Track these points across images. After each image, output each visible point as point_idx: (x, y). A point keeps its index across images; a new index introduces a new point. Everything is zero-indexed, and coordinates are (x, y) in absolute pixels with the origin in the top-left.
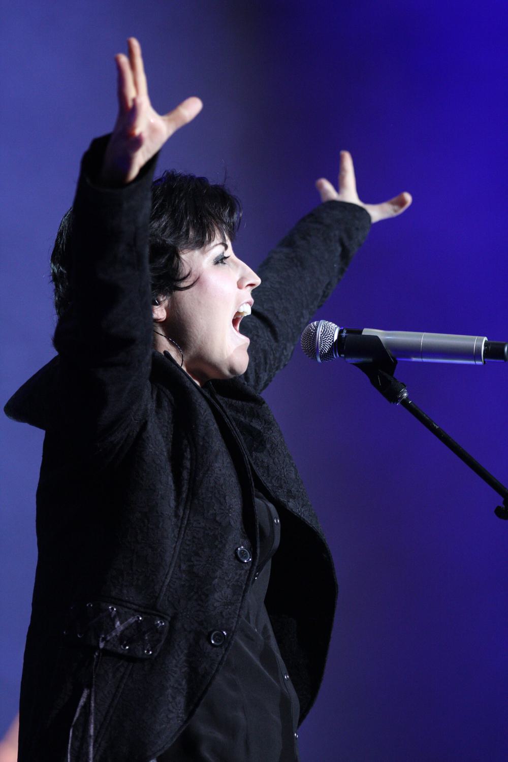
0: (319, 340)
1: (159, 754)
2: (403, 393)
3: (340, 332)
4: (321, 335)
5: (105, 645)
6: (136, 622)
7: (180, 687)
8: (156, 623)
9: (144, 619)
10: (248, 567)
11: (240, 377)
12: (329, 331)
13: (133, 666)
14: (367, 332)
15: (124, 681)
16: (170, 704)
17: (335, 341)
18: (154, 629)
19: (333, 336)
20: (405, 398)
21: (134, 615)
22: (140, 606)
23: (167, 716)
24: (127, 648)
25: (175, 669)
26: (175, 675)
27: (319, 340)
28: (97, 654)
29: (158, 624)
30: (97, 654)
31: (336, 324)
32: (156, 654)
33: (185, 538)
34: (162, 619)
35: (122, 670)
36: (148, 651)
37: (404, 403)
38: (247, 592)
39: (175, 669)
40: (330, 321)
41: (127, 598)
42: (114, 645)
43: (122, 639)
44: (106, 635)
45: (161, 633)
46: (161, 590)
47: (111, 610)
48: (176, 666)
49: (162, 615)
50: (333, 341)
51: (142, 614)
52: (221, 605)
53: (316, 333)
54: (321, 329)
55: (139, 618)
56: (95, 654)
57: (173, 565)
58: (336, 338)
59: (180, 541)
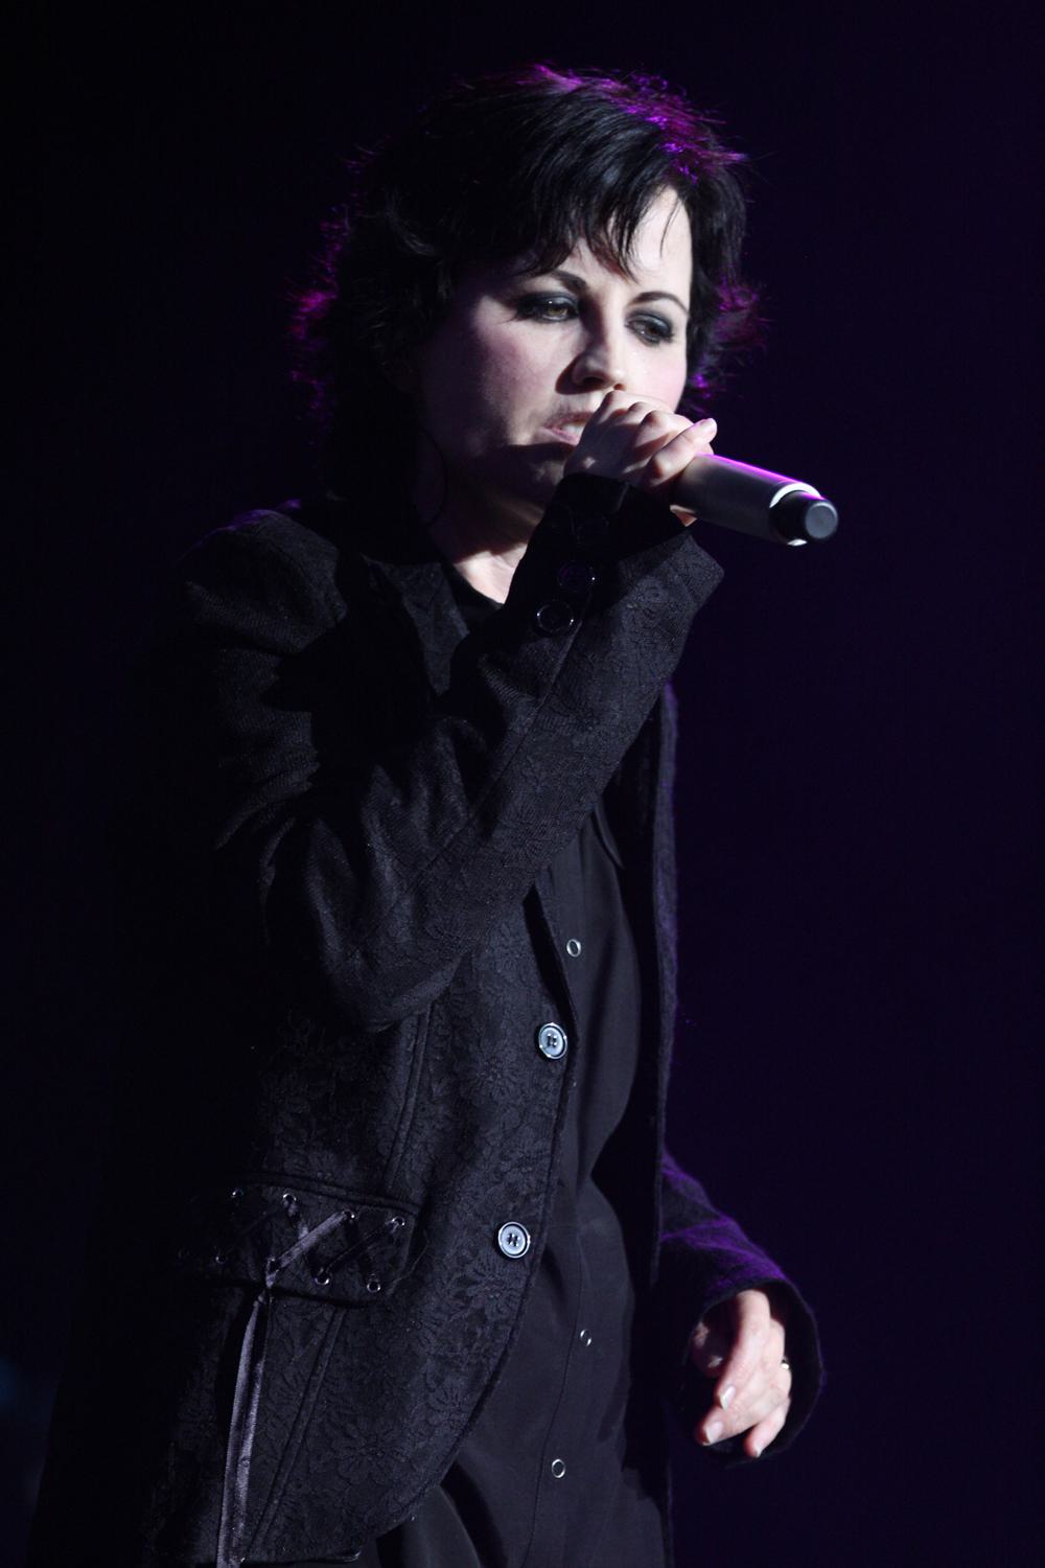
1: (559, 431)
5: (277, 1280)
6: (344, 1223)
7: (450, 1355)
8: (387, 1223)
9: (362, 1217)
10: (558, 1070)
11: (586, 362)
13: (345, 1315)
15: (328, 1351)
16: (431, 1395)
18: (382, 1234)
21: (339, 1211)
22: (349, 1189)
23: (426, 1421)
24: (327, 1282)
25: (438, 1316)
26: (439, 1330)
28: (261, 1299)
29: (392, 1225)
30: (261, 1299)
32: (390, 1291)
33: (435, 1024)
34: (401, 1213)
35: (322, 1327)
36: (374, 1286)
38: (562, 1128)
39: (438, 1316)
41: (319, 1174)
42: (298, 1278)
43: (312, 1258)
44: (277, 1256)
45: (399, 1244)
46: (393, 1151)
47: (286, 1203)
48: (439, 1309)
49: (400, 1204)
52: (512, 1167)
55: (349, 1215)
56: (257, 1299)
57: (415, 1090)
59: (425, 1029)
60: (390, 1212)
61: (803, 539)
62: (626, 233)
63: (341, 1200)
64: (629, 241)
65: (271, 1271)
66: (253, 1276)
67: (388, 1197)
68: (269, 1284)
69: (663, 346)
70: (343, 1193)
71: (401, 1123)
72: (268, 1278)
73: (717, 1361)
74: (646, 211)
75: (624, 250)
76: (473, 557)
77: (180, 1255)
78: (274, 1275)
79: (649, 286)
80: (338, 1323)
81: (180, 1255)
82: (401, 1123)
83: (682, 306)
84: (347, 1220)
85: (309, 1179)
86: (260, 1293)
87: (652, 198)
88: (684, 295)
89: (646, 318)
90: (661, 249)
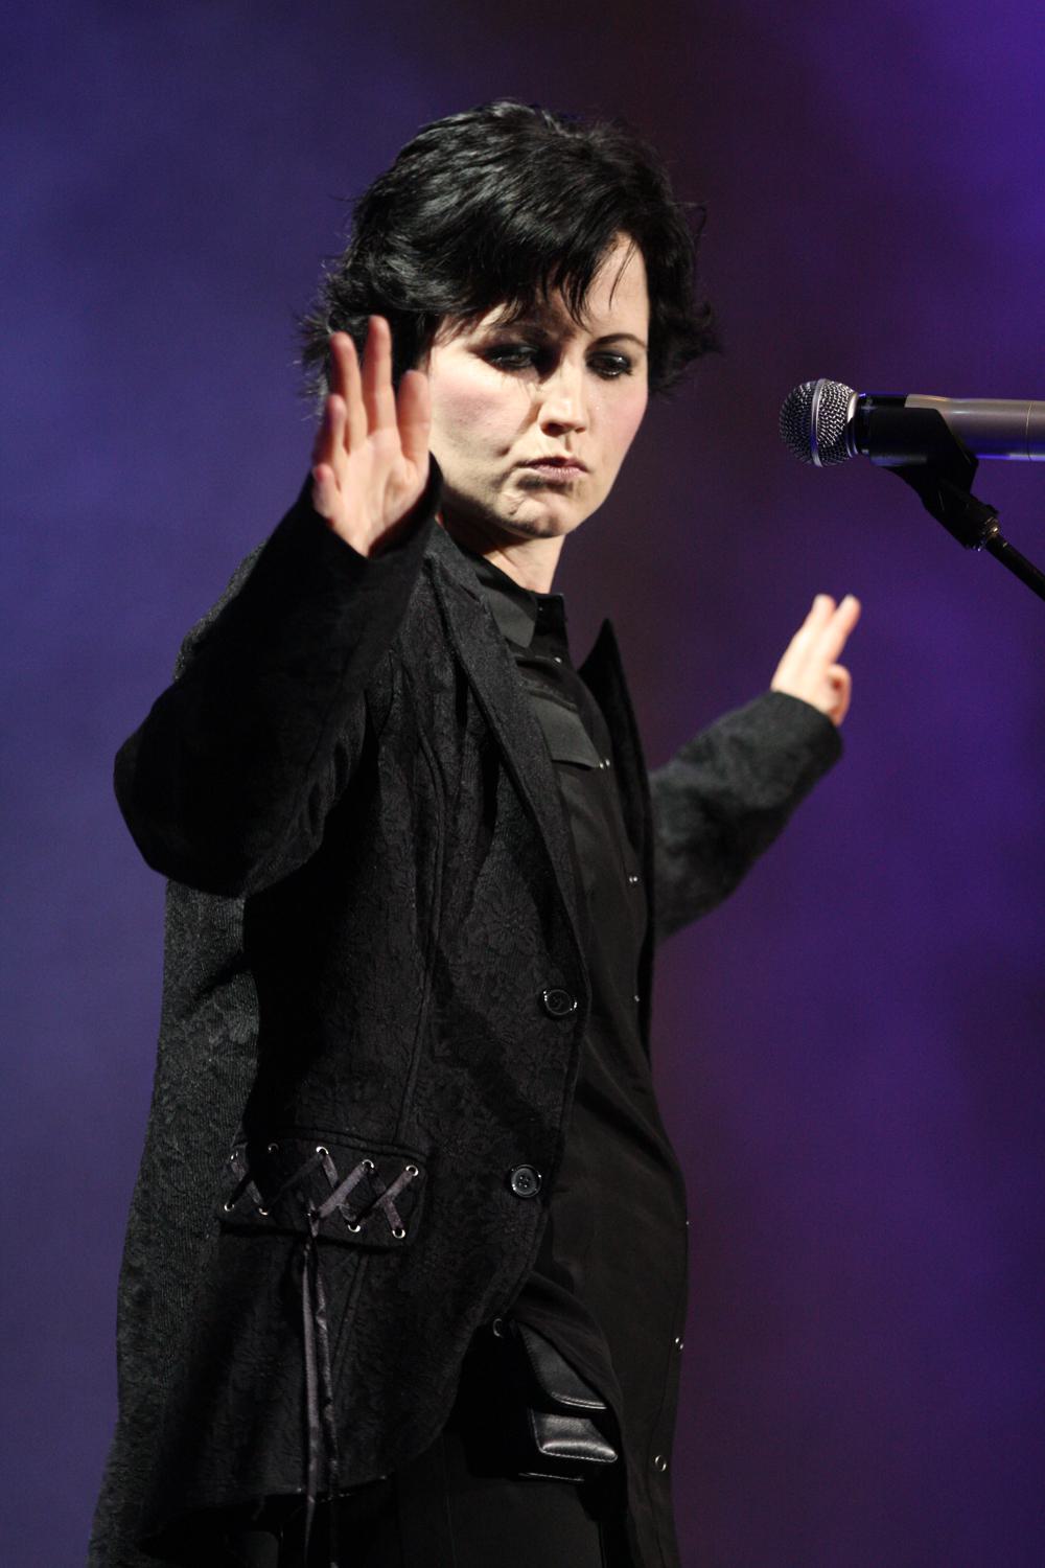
0: (817, 419)
2: (992, 525)
3: (860, 402)
4: (821, 409)
5: (320, 1229)
12: (835, 401)
14: (915, 401)
17: (849, 420)
19: (846, 412)
20: (994, 535)
27: (817, 419)
28: (308, 1247)
30: (308, 1247)
31: (851, 387)
37: (994, 546)
40: (847, 384)
50: (845, 421)
51: (373, 1156)
53: (810, 405)
54: (820, 397)
58: (851, 415)
60: (403, 1160)
61: (615, 1449)
62: (579, 289)
63: (363, 1150)
64: (582, 293)
65: (314, 1222)
66: (298, 1225)
67: (402, 1147)
68: (315, 1234)
69: (624, 378)
70: (363, 1145)
71: (408, 1080)
72: (313, 1229)
73: (867, 408)
74: (604, 263)
75: (577, 305)
76: (461, 491)
77: (323, 266)
78: (317, 1225)
79: (605, 332)
80: (364, 1262)
81: (323, 266)
82: (408, 1080)
83: (639, 342)
84: (368, 1173)
85: (338, 1133)
86: (305, 1243)
87: (604, 252)
88: (642, 332)
89: (605, 357)
90: (611, 297)
